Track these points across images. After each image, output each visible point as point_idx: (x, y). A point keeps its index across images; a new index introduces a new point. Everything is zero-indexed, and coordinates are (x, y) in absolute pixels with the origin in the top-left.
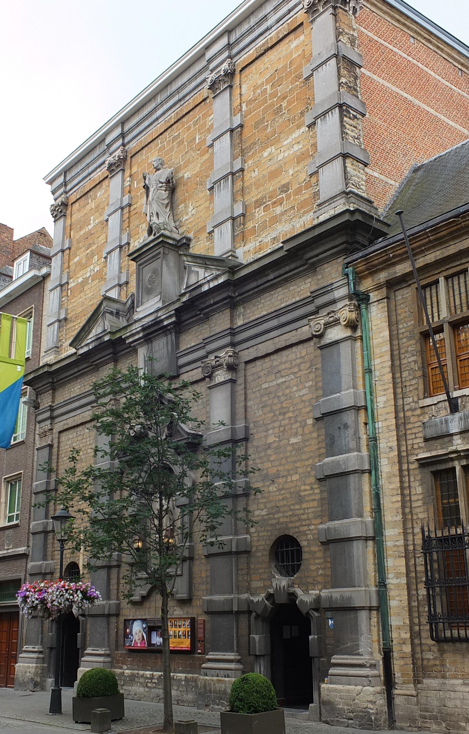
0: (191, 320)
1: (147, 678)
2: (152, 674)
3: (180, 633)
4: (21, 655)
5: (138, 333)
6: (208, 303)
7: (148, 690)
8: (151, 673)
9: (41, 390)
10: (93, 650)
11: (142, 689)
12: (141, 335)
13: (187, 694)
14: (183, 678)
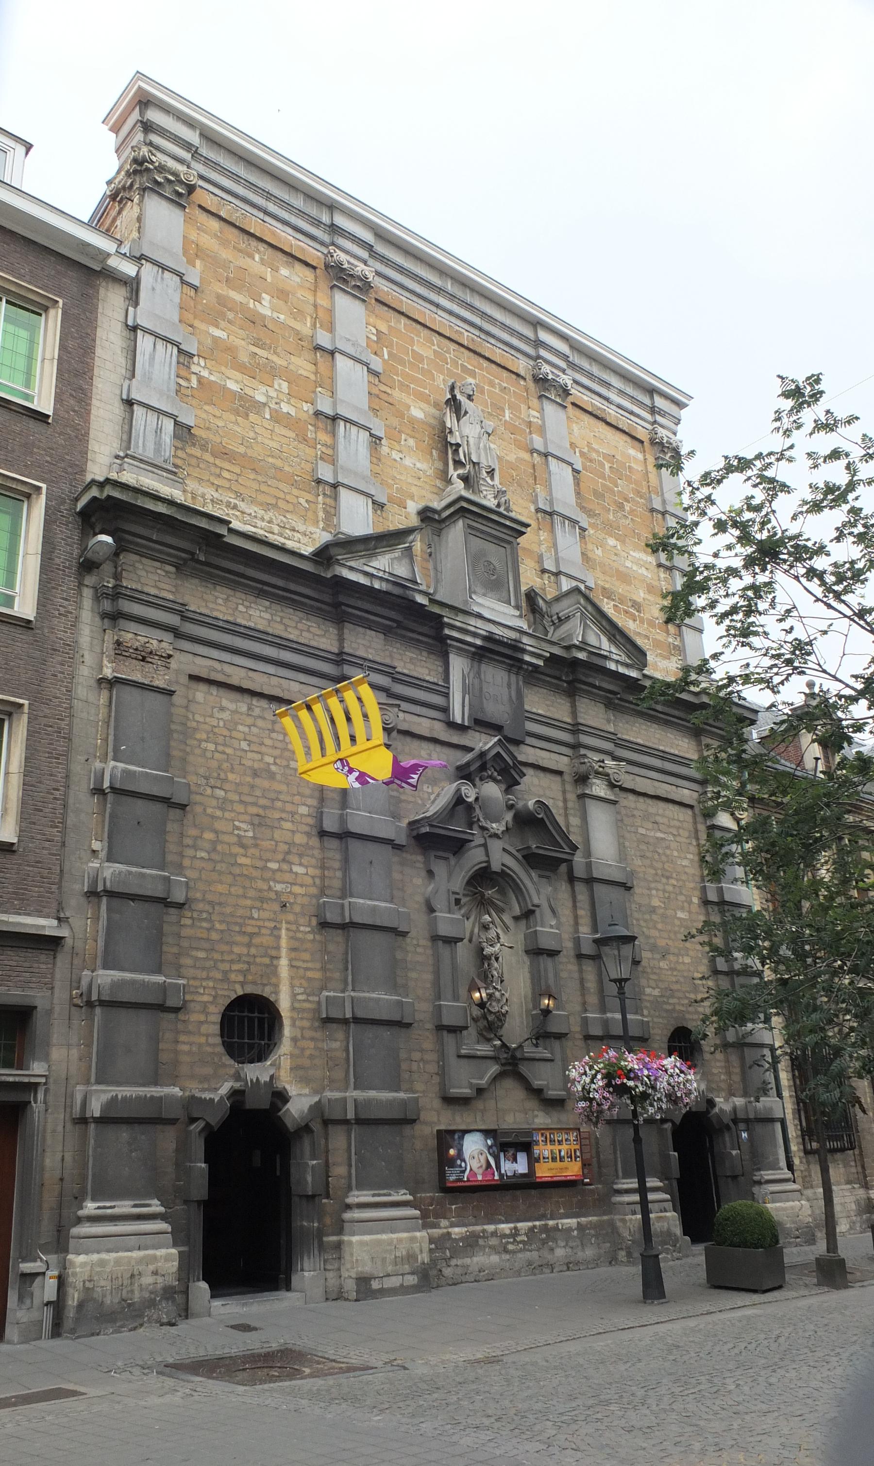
0: (548, 679)
1: (504, 1236)
2: (516, 1228)
3: (563, 1153)
4: (75, 1231)
5: (475, 635)
6: (590, 680)
7: (508, 1257)
8: (512, 1225)
9: (137, 544)
10: (374, 1195)
11: (495, 1259)
12: (479, 642)
13: (583, 1250)
14: (575, 1226)
